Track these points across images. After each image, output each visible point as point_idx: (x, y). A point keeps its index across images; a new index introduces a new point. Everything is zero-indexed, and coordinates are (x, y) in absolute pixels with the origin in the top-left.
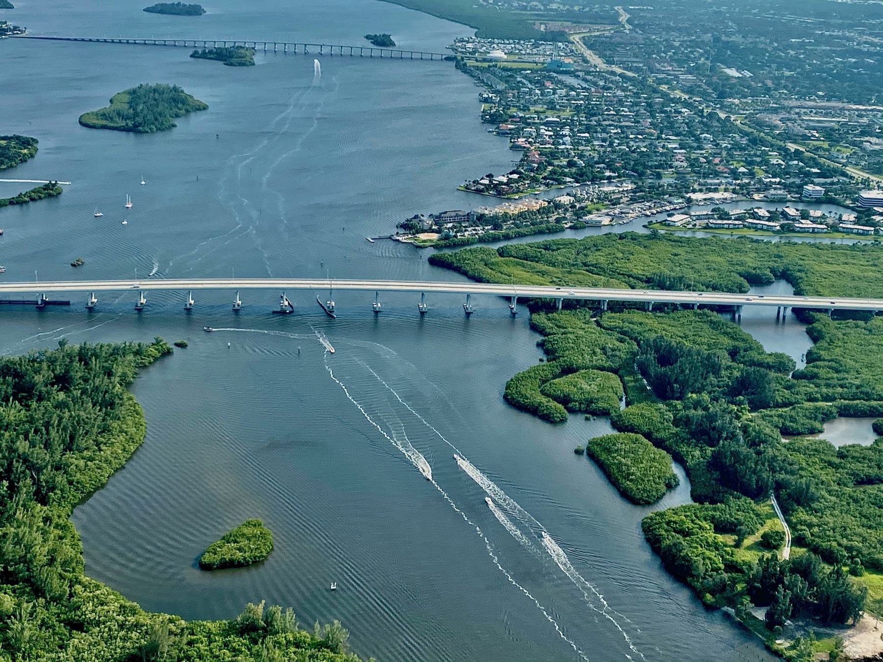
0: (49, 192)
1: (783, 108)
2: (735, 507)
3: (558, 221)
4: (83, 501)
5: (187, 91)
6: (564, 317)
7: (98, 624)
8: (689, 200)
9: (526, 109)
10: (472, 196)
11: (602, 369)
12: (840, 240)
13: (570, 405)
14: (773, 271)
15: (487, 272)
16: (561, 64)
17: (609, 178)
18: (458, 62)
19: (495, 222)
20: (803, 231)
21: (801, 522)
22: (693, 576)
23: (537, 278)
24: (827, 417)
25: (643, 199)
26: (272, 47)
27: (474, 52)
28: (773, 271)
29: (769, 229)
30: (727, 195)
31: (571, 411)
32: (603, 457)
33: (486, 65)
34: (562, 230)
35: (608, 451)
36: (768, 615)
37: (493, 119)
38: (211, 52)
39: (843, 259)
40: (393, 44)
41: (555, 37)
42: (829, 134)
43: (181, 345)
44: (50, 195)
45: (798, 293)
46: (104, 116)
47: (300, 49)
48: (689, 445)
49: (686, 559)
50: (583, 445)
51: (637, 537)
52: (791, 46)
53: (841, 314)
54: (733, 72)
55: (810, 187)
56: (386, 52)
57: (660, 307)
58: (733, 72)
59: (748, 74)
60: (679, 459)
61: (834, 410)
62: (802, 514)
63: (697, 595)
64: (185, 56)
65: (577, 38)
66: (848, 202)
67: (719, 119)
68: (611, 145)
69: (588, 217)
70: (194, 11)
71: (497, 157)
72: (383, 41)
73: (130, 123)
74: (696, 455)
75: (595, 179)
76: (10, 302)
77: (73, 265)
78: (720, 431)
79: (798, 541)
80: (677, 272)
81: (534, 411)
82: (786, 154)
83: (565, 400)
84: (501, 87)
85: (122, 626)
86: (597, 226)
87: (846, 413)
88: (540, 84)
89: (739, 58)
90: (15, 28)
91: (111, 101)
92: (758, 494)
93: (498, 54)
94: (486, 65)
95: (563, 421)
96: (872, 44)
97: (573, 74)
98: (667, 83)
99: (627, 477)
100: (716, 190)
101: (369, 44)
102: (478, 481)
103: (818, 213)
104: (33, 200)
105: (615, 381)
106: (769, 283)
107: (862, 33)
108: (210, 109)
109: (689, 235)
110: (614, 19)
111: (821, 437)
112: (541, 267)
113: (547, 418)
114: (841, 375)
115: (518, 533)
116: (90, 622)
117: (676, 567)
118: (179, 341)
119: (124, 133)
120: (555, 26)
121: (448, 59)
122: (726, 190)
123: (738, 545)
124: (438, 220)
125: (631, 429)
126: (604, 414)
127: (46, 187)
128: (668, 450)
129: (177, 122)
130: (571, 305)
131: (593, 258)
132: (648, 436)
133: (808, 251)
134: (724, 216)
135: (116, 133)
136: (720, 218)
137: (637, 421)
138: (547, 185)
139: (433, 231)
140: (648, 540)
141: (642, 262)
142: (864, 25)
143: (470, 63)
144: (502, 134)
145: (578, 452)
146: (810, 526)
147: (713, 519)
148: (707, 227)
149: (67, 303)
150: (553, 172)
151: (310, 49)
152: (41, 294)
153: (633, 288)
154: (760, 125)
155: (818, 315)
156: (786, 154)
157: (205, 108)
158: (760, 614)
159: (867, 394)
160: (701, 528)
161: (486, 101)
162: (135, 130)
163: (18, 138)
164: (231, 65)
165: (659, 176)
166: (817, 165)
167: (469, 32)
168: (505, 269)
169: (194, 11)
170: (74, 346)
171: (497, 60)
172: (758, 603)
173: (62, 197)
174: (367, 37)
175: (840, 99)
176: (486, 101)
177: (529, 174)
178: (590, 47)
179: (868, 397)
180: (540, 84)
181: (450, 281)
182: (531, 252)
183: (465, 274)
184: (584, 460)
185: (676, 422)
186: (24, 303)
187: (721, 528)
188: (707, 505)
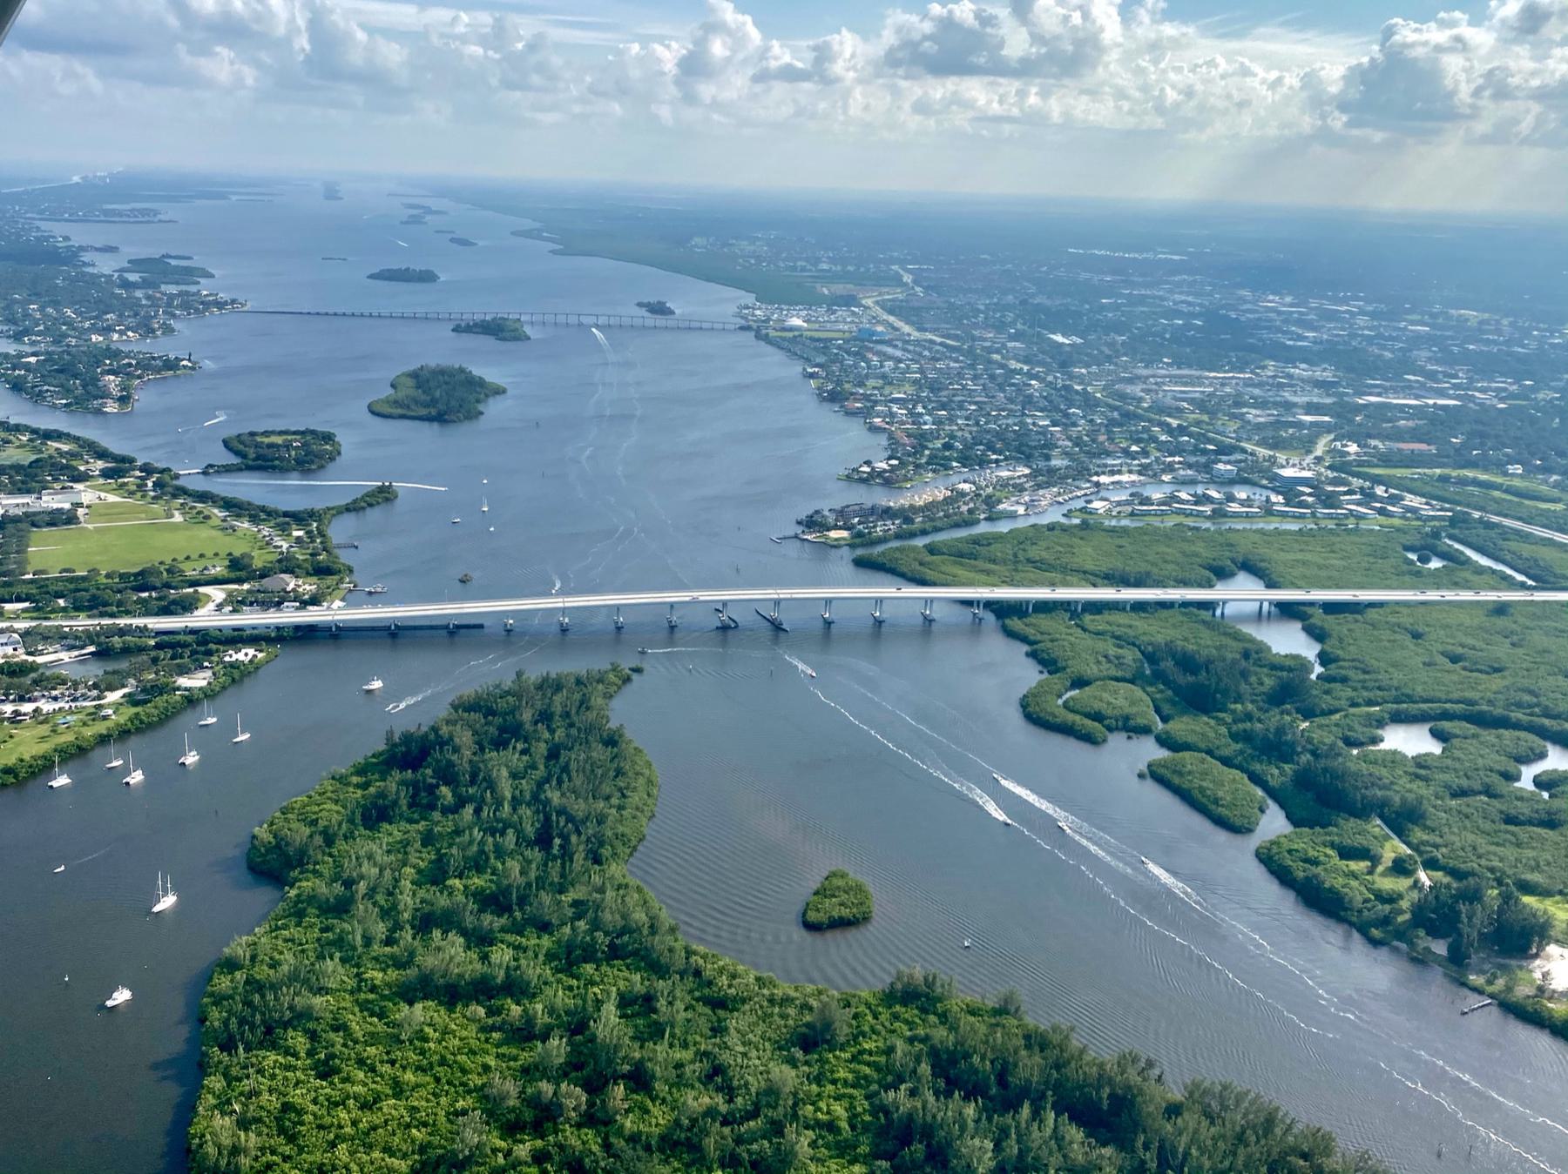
0: (384, 495)
1: (1139, 378)
2: (1350, 830)
3: (970, 511)
4: (631, 855)
5: (477, 371)
6: (1043, 621)
7: (744, 1001)
8: (1097, 484)
9: (861, 384)
10: (854, 485)
11: (1117, 679)
12: (1273, 525)
13: (1107, 722)
14: (1233, 561)
15: (930, 574)
16: (874, 333)
17: (997, 461)
18: (758, 331)
19: (905, 515)
20: (1236, 515)
21: (1423, 843)
22: (1346, 909)
23: (983, 577)
24: (1381, 724)
25: (1048, 485)
26: (540, 318)
27: (768, 320)
28: (1233, 561)
29: (1199, 514)
30: (1134, 477)
31: (1110, 729)
32: (1176, 780)
33: (790, 334)
34: (978, 522)
35: (1181, 774)
36: (1451, 949)
37: (834, 397)
38: (476, 325)
39: (1296, 546)
40: (672, 313)
41: (849, 301)
42: (1201, 405)
43: (638, 670)
44: (387, 500)
45: (1271, 585)
46: (396, 403)
47: (573, 320)
48: (1261, 762)
49: (1331, 890)
50: (1143, 767)
51: (1258, 873)
52: (1103, 308)
53: (1331, 608)
54: (1059, 338)
55: (1221, 466)
56: (661, 321)
57: (1139, 606)
58: (1059, 338)
59: (1079, 341)
60: (1256, 779)
61: (1387, 716)
62: (1418, 835)
63: (1363, 930)
64: (446, 330)
65: (869, 302)
66: (1265, 482)
67: (1077, 392)
68: (977, 424)
69: (1001, 507)
70: (427, 277)
71: (849, 444)
72: (659, 309)
73: (434, 412)
74: (1277, 774)
75: (983, 463)
76: (415, 628)
77: (462, 581)
78: (1292, 745)
79: (1430, 864)
80: (1144, 567)
81: (1066, 730)
82: (1169, 430)
83: (1097, 717)
84: (821, 359)
85: (771, 1001)
86: (1012, 516)
87: (1399, 719)
88: (860, 355)
89: (1061, 321)
90: (233, 302)
91: (392, 386)
92: (1362, 811)
93: (796, 322)
94: (790, 334)
95: (1105, 741)
96: (1189, 304)
97: (889, 343)
98: (998, 351)
99: (1216, 801)
100: (1120, 472)
101: (643, 312)
102: (1050, 812)
103: (1243, 496)
104: (371, 505)
105: (1138, 692)
106: (1232, 575)
107: (1171, 291)
108: (509, 393)
109: (1114, 523)
110: (898, 281)
111: (1382, 746)
112: (980, 564)
113: (1089, 739)
114: (1373, 676)
115: (1129, 871)
116: (734, 999)
117: (1320, 900)
118: (633, 666)
119: (426, 424)
120: (840, 289)
121: (742, 328)
122: (1130, 472)
123: (1371, 872)
124: (841, 513)
125: (1186, 747)
126: (1145, 730)
127: (381, 489)
128: (1243, 770)
129: (481, 407)
130: (1044, 607)
131: (1035, 552)
132: (1209, 752)
133: (1257, 537)
134: (1146, 501)
135: (417, 423)
136: (1141, 504)
137: (1191, 739)
138: (934, 471)
139: (840, 528)
140: (1272, 872)
141: (1087, 554)
142: (1167, 282)
143: (772, 333)
144: (850, 414)
145: (1141, 776)
146: (1436, 846)
147: (1333, 845)
148: (1132, 514)
149: (481, 626)
150: (931, 457)
151: (584, 320)
152: (394, 618)
153: (1095, 586)
154: (1123, 397)
155: (1310, 610)
156: (1169, 430)
157: (504, 391)
158: (1440, 948)
159: (1408, 696)
160: (1326, 855)
161: (812, 376)
162: (441, 418)
163: (313, 432)
164: (504, 339)
165: (1048, 458)
166: (1210, 441)
167: (750, 299)
168: (943, 568)
169: (427, 277)
170: (533, 675)
171: (798, 329)
172: (1434, 933)
173: (398, 502)
174: (640, 305)
175: (1190, 367)
176: (812, 376)
177: (917, 455)
178: (891, 312)
179: (1410, 699)
180: (860, 355)
181: (878, 585)
182: (965, 548)
183: (903, 576)
184: (1149, 783)
185: (1235, 737)
186: (373, 629)
187: (1347, 853)
188: (1318, 829)
